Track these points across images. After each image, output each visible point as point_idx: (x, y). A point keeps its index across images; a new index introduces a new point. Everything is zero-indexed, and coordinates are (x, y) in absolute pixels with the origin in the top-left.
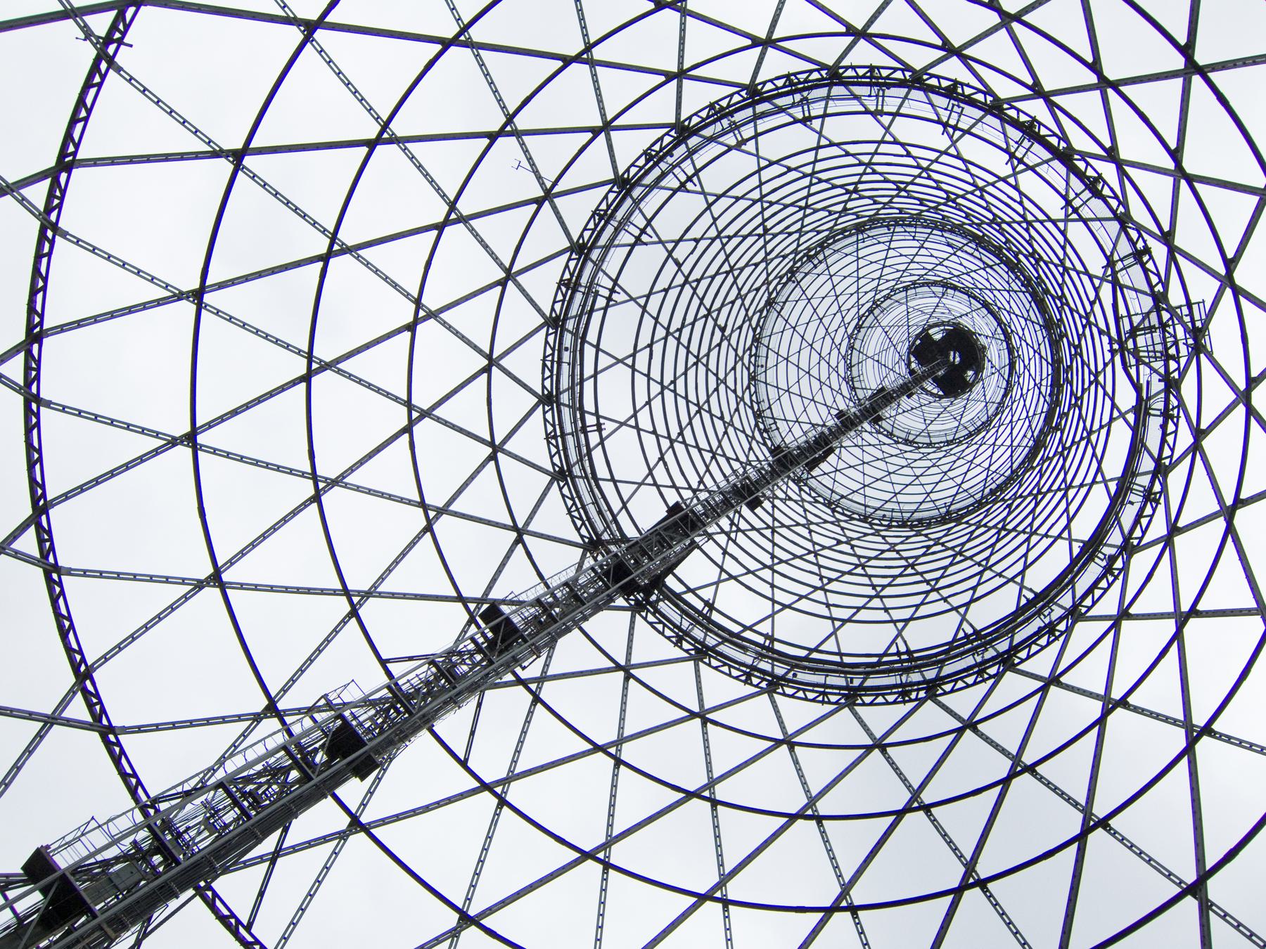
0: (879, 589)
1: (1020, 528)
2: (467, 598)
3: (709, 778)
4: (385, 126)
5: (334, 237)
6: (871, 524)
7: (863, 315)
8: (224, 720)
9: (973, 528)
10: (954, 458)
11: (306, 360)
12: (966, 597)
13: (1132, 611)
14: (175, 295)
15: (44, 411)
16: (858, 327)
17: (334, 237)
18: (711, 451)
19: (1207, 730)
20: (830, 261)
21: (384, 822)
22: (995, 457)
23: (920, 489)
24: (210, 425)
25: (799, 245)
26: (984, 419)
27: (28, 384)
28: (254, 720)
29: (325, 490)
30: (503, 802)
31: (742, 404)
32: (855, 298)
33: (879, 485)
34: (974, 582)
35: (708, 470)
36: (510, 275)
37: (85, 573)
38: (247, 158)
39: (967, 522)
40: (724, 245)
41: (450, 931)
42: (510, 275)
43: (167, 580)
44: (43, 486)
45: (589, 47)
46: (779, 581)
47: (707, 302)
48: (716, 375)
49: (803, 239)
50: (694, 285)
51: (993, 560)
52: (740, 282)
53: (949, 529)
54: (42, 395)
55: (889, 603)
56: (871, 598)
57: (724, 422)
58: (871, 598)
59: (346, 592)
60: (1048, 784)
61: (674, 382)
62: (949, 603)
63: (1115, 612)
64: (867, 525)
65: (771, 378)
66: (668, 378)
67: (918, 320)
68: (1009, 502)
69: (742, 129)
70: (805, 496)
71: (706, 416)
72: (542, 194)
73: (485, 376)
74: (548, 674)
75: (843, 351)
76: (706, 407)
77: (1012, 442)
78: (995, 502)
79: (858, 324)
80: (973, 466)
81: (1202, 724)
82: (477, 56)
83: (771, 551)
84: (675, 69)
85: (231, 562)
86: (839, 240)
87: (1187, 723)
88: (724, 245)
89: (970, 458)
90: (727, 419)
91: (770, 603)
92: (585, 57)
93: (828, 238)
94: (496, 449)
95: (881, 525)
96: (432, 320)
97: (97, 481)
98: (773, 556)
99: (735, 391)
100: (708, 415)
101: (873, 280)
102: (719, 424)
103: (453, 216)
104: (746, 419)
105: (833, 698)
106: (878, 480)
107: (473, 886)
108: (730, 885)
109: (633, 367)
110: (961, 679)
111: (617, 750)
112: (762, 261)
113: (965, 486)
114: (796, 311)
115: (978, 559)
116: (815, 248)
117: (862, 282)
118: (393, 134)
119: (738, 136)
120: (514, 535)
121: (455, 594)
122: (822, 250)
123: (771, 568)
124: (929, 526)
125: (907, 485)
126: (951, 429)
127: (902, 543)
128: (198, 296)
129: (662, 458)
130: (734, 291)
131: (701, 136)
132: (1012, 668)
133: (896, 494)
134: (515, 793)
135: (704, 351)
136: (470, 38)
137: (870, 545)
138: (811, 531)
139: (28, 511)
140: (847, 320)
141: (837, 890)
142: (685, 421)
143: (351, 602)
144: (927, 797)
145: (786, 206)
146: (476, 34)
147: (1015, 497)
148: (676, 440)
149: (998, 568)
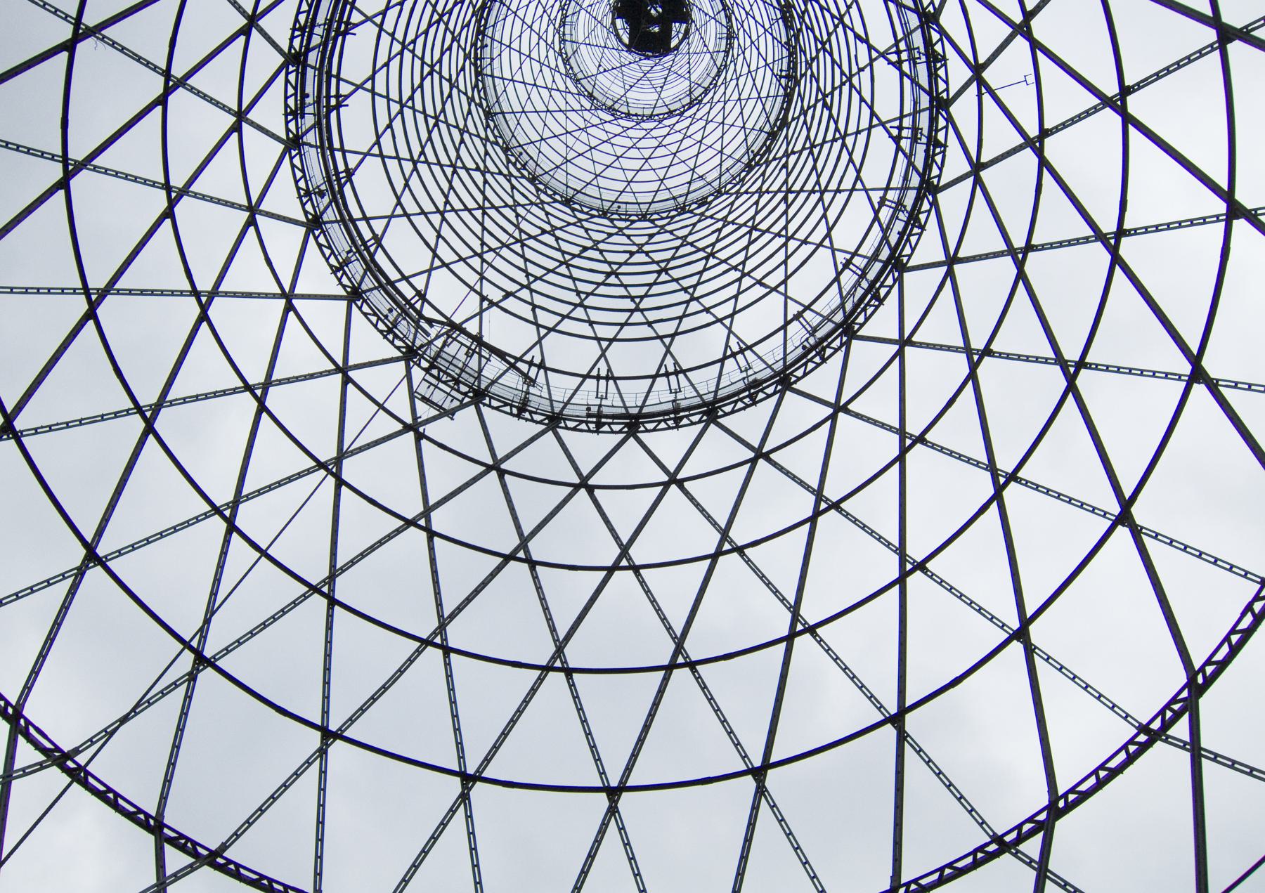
0: (783, 233)
1: (831, 28)
2: (512, 553)
3: (812, 493)
4: (86, 290)
5: (139, 409)
6: (726, 193)
7: (560, 49)
8: (443, 824)
9: (802, 118)
10: (734, 82)
11: (217, 516)
12: (851, 173)
13: (981, 60)
14: (76, 575)
15: (226, 854)
16: (566, 61)
17: (139, 409)
18: (561, 263)
19: (1125, 91)
20: (497, 37)
21: (629, 769)
22: (762, 50)
23: (734, 130)
24: (325, 712)
25: (464, 50)
26: (725, 30)
27: (195, 854)
28: (463, 801)
29: (332, 590)
30: (692, 665)
31: (546, 206)
32: (542, 43)
33: (701, 158)
34: (845, 156)
35: (574, 279)
36: (289, 297)
37: (237, 835)
38: (15, 423)
39: (793, 119)
40: (413, 108)
41: (757, 792)
42: (289, 297)
43: (297, 775)
44: (140, 811)
45: (167, 74)
46: (708, 302)
47: (445, 161)
48: (507, 205)
49: (462, 43)
50: (422, 159)
51: (842, 127)
52: (451, 121)
53: (786, 137)
54: (213, 848)
55: (801, 235)
56: (785, 245)
57: (548, 233)
58: (785, 245)
59: (426, 643)
60: (1052, 246)
61: (483, 244)
62: (844, 191)
63: (970, 74)
64: (725, 196)
65: (547, 166)
66: (476, 245)
67: (695, 38)
68: (809, 73)
69: (892, 210)
70: (659, 223)
71: (531, 243)
72: (248, 214)
73: (350, 386)
74: (625, 543)
75: (574, 90)
76: (568, 257)
77: (763, 27)
78: (798, 83)
79: (563, 60)
80: (754, 74)
81: (1117, 91)
82: (95, 169)
83: (679, 287)
84: (244, 21)
85: (325, 712)
86: (780, 113)
87: (1106, 101)
88: (413, 108)
89: (745, 70)
90: (548, 228)
91: (719, 324)
92: (172, 84)
93: (479, 21)
94: (496, 467)
95: (735, 185)
96: (271, 389)
97: (172, 764)
98: (685, 290)
99: (610, 235)
100: (532, 240)
101: (542, 16)
102: (546, 238)
103: (204, 299)
104: (560, 214)
105: (890, 281)
106: (697, 155)
107: (737, 745)
108: (910, 551)
109: (445, 265)
110: (309, 12)
111: (730, 543)
112: (451, 89)
113: (764, 94)
114: (513, 98)
115: (830, 137)
116: (477, 39)
117: (536, 27)
118: (98, 290)
119: (854, 269)
120: (494, 474)
121: (500, 560)
122: (484, 36)
123: (692, 299)
124: (769, 150)
125: (722, 137)
126: (709, 62)
127: (763, 182)
128: (92, 557)
129: (534, 307)
130: (455, 132)
131: (314, 48)
132: (936, 190)
133: (721, 152)
134: (694, 649)
135: (480, 198)
136: (75, 161)
137: (744, 209)
138: (692, 244)
139: (151, 838)
140: (553, 66)
141: (987, 475)
142: (520, 262)
143: (436, 645)
144: (978, 343)
145: (421, 86)
146: (77, 152)
147: (809, 66)
148: (582, 301)
149: (852, 128)
